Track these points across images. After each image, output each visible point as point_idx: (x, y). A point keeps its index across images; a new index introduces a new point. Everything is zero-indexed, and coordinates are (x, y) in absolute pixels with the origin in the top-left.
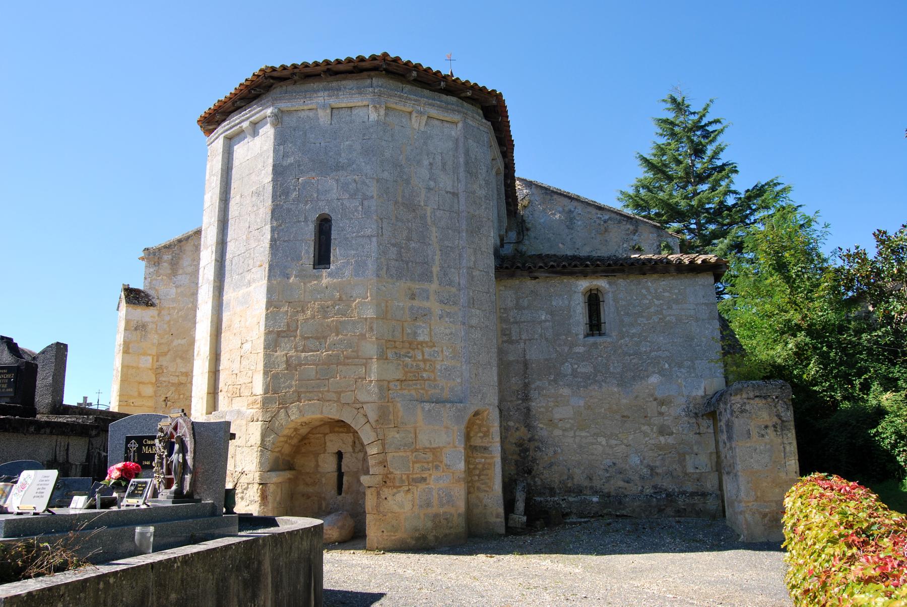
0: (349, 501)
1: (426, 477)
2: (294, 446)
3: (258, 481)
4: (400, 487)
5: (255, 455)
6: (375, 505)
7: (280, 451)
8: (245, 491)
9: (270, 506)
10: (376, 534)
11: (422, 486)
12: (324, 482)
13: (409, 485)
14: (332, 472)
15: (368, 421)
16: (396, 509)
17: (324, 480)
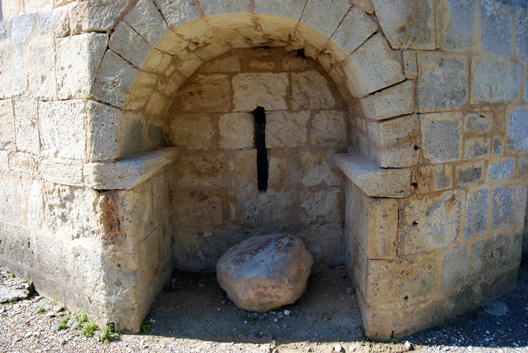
0: (284, 203)
1: (480, 168)
2: (170, 98)
3: (94, 184)
4: (439, 193)
5: (80, 119)
6: (393, 239)
7: (142, 110)
8: (68, 204)
9: (130, 244)
10: (393, 305)
11: (473, 188)
12: (232, 168)
13: (455, 187)
14: (248, 148)
15: (379, 31)
16: (431, 243)
17: (231, 164)
